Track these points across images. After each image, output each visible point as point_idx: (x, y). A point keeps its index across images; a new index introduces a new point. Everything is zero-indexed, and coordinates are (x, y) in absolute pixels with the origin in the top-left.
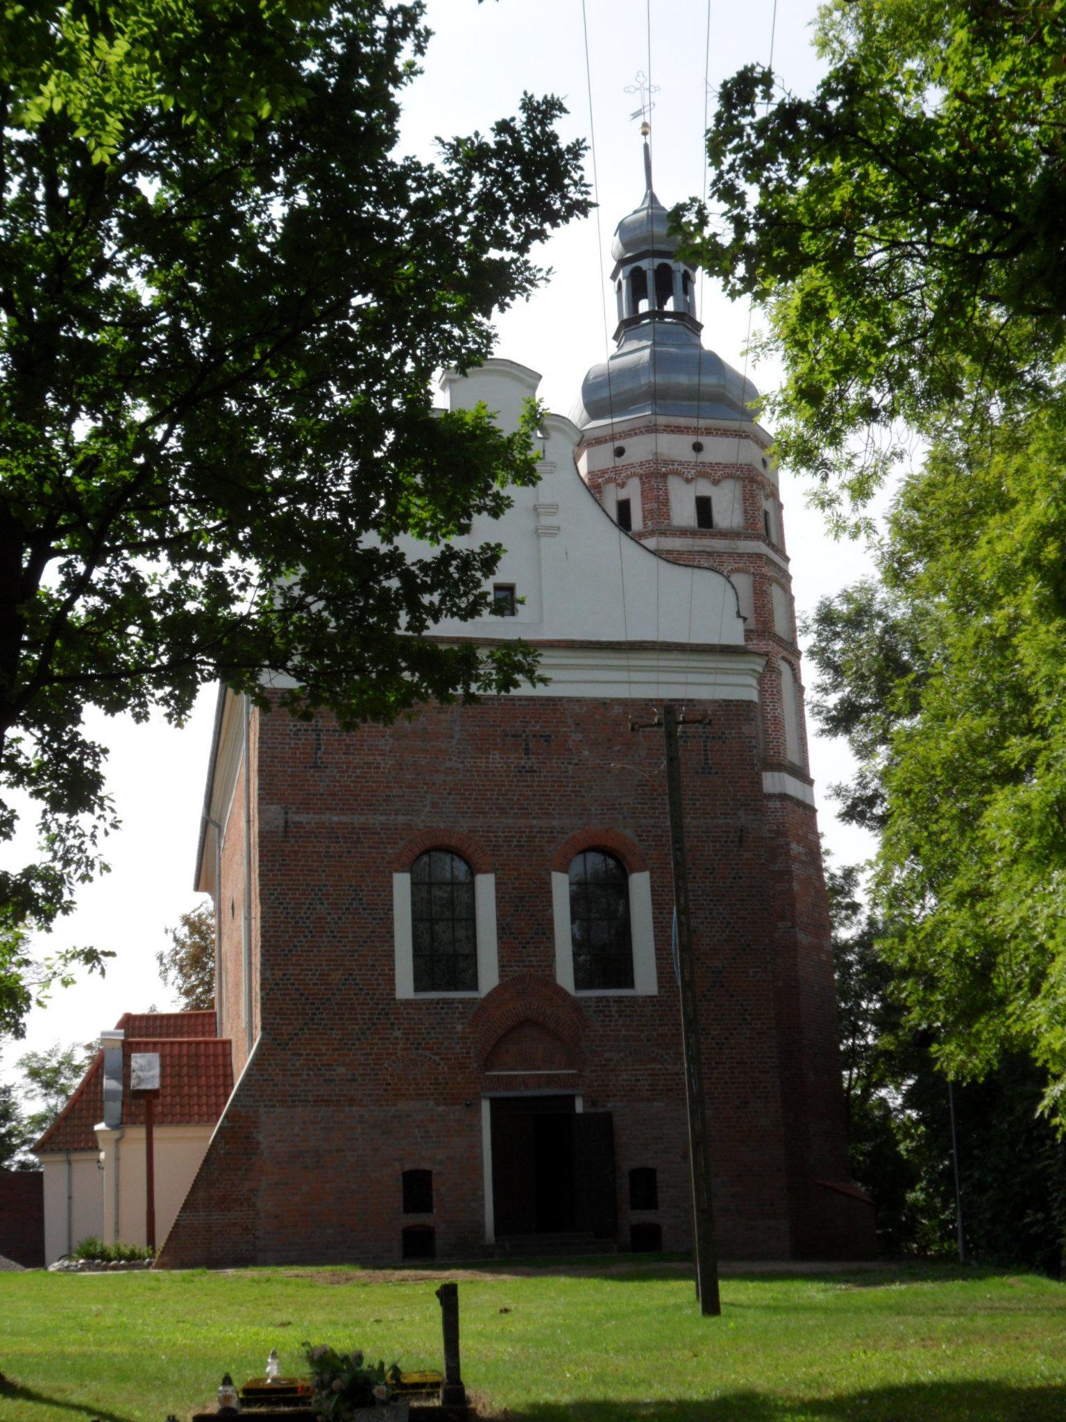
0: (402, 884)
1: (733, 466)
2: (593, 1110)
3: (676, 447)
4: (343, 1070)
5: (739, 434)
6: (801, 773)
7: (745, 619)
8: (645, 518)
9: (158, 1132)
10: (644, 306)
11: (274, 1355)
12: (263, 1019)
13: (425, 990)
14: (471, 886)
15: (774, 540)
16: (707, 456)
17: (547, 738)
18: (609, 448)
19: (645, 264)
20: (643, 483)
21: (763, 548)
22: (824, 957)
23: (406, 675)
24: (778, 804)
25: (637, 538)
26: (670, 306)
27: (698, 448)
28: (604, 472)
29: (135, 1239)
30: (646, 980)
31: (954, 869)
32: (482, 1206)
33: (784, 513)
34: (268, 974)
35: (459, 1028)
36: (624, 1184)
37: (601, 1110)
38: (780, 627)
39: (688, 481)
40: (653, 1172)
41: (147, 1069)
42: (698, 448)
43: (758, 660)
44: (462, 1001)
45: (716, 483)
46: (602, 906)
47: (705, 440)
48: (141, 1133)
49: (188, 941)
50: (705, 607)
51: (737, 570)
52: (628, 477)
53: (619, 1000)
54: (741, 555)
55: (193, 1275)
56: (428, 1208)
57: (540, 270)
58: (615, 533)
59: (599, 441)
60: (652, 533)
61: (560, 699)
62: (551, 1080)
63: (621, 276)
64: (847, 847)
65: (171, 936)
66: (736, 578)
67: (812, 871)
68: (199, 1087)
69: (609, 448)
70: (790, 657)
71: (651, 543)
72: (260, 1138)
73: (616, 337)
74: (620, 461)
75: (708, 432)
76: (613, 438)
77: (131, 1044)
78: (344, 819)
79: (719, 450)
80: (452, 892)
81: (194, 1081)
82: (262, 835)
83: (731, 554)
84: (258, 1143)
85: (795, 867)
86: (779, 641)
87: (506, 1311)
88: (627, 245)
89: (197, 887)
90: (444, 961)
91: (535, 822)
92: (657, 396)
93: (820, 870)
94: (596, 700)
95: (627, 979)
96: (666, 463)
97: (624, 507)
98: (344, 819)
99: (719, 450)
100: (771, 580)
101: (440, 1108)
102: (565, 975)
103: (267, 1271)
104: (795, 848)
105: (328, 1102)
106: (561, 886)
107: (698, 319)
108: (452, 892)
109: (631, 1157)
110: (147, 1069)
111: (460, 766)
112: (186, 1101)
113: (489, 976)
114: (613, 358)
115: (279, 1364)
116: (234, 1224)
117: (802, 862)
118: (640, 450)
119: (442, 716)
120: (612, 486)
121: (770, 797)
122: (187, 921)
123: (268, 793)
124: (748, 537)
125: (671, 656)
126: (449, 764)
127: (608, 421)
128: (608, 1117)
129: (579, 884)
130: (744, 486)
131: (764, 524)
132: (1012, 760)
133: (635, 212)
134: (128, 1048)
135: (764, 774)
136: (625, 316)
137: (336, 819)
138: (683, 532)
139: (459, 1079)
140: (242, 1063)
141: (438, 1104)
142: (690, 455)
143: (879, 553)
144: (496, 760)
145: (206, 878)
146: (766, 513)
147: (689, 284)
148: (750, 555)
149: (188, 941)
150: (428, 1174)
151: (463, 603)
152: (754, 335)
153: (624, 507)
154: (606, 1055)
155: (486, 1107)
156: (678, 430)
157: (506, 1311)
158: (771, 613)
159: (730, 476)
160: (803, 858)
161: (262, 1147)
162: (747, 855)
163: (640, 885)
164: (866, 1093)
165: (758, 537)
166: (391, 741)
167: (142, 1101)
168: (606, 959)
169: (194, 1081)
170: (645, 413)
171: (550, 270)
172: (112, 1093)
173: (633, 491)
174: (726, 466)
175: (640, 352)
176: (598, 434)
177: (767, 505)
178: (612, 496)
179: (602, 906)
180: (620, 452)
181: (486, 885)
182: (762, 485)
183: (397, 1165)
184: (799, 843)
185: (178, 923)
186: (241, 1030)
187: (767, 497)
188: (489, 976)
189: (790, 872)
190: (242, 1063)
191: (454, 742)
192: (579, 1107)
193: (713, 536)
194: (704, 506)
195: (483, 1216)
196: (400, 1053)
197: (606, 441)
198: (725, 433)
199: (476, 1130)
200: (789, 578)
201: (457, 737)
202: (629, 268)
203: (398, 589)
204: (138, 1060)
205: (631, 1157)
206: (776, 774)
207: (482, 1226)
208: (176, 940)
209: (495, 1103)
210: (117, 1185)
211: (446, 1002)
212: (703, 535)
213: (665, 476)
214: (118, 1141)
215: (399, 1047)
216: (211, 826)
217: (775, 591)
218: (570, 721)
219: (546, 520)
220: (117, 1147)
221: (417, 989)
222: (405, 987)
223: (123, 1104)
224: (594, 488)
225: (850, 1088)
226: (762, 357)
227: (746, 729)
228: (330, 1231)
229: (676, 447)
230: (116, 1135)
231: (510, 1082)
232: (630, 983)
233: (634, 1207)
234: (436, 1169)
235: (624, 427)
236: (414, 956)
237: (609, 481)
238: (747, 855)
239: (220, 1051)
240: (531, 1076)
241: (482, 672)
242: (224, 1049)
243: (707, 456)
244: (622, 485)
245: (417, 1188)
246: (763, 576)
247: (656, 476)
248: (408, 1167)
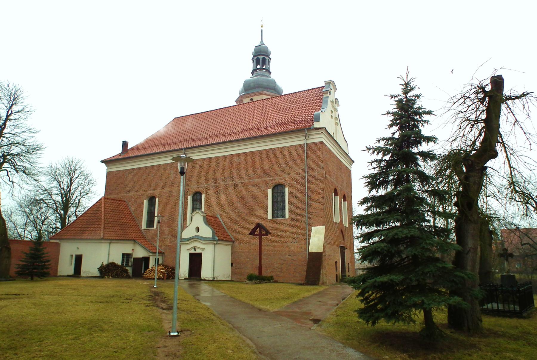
10: (258, 67)
26: (264, 67)
135: (324, 227)
202: (256, 58)
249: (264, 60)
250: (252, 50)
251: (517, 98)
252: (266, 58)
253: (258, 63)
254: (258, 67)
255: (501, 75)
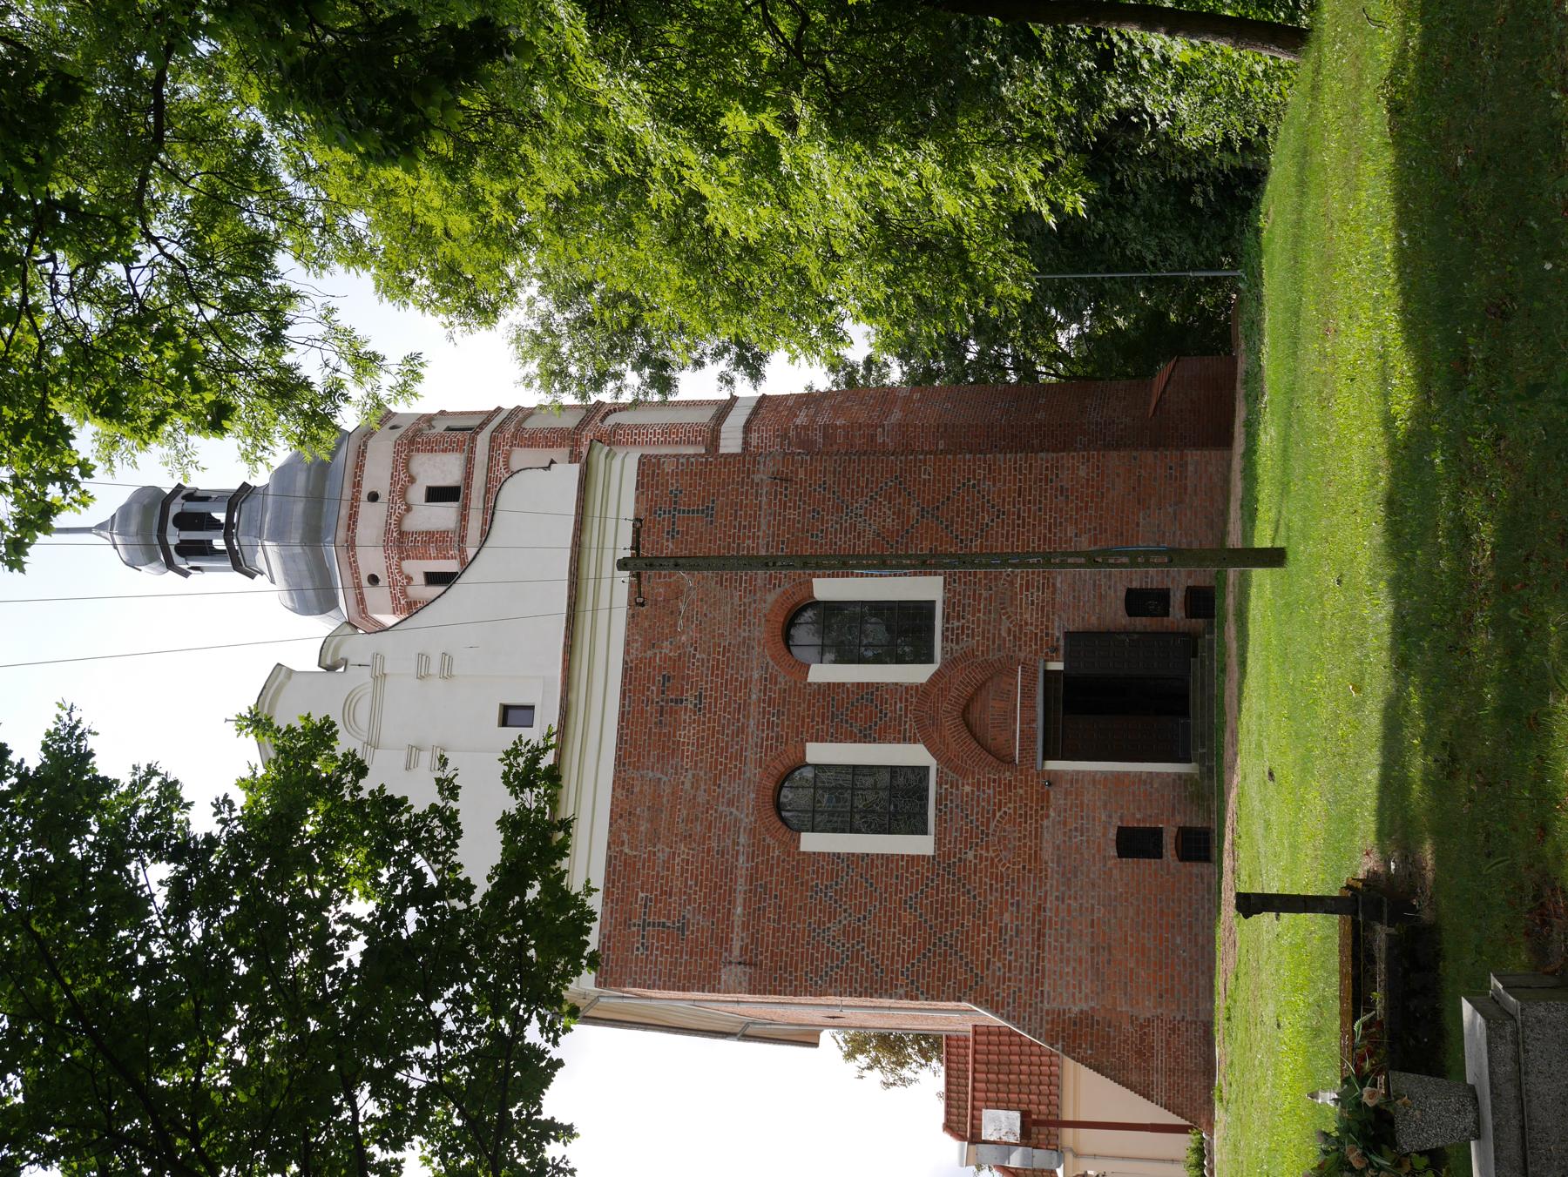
0: (812, 842)
1: (395, 461)
2: (1062, 652)
3: (372, 520)
4: (1007, 916)
5: (361, 453)
6: (724, 409)
7: (552, 462)
8: (445, 558)
9: (1068, 1116)
10: (219, 544)
11: (1313, 1096)
12: (948, 1000)
13: (925, 823)
14: (820, 768)
15: (476, 422)
16: (383, 490)
17: (666, 678)
18: (370, 592)
19: (174, 537)
20: (408, 557)
21: (483, 440)
22: (916, 396)
23: (532, 894)
24: (754, 435)
25: (466, 565)
26: (221, 516)
27: (374, 497)
28: (394, 598)
29: (1182, 1144)
30: (926, 588)
31: (801, 271)
32: (1158, 774)
33: (449, 410)
34: (901, 991)
35: (967, 789)
36: (1141, 623)
37: (1062, 643)
38: (570, 422)
39: (409, 509)
40: (1130, 591)
41: (1000, 1123)
42: (374, 497)
43: (595, 453)
44: (939, 784)
45: (412, 480)
46: (848, 631)
47: (366, 489)
48: (1068, 1135)
49: (873, 1054)
50: (540, 497)
51: (507, 464)
52: (401, 572)
53: (947, 618)
54: (490, 458)
55: (1221, 1099)
56: (1157, 833)
57: (59, 717)
58: (457, 589)
59: (361, 601)
60: (462, 551)
61: (625, 662)
62: (1028, 694)
63: (185, 567)
64: (792, 374)
65: (866, 1072)
66: (514, 466)
67: (826, 404)
68: (1021, 1063)
69: (370, 592)
70: (602, 414)
71: (471, 552)
72: (1076, 1009)
73: (252, 576)
74: (383, 581)
75: (357, 485)
76: (359, 586)
77: (972, 1135)
78: (740, 901)
79: (378, 475)
80: (824, 788)
81: (1015, 1068)
82: (753, 991)
83: (489, 470)
84: (1081, 1012)
85: (820, 421)
86: (583, 424)
87: (1271, 774)
88: (152, 559)
89: (816, 1045)
90: (897, 801)
91: (754, 697)
92: (314, 536)
93: (827, 395)
94: (628, 624)
95: (923, 610)
96: (388, 531)
97: (433, 579)
98: (740, 901)
99: (378, 475)
100: (519, 429)
101: (1052, 814)
102: (917, 674)
103: (1220, 1002)
104: (801, 419)
105: (1041, 935)
106: (824, 673)
107: (236, 487)
108: (824, 788)
109: (1114, 614)
110: (1000, 1123)
111: (690, 773)
112: (1035, 1079)
113: (914, 754)
114: (273, 581)
115: (1324, 1091)
116: (1168, 1042)
117: (816, 413)
118: (372, 559)
119: (637, 790)
120: (411, 591)
121: (746, 443)
122: (850, 1056)
123: (708, 981)
124: (472, 450)
125: (587, 544)
126: (688, 785)
127: (340, 592)
128: (1068, 635)
129: (823, 649)
130: (418, 450)
131: (459, 432)
132: (673, 201)
133: (115, 546)
134: (975, 1139)
135: (722, 451)
136: (229, 564)
137: (739, 910)
138: (463, 517)
139: (1021, 791)
140: (996, 1021)
141: (1048, 816)
142: (380, 508)
143: (458, 329)
144: (687, 734)
145: (807, 1038)
146: (449, 429)
147: (198, 494)
148: (491, 449)
149: (873, 1054)
150: (1121, 831)
151: (440, 833)
152: (166, 464)
153: (433, 579)
154: (1004, 634)
155: (1052, 765)
156: (353, 517)
157: (1271, 774)
158: (553, 430)
159: (407, 465)
160: (812, 412)
161: (1085, 1008)
162: (801, 475)
163: (827, 589)
164: (1063, 356)
165: (473, 440)
166: (659, 846)
167: (1034, 1129)
168: (904, 630)
169: (1015, 1068)
170: (332, 553)
171: (60, 706)
172: (1024, 1157)
173: (417, 568)
174: (395, 468)
175: (268, 554)
176: (352, 602)
177: (440, 427)
178: (420, 590)
179: (848, 631)
180: (374, 580)
181: (820, 753)
182: (418, 432)
183: (1110, 863)
184: (796, 416)
185: (852, 1067)
186: (960, 1018)
187: (431, 427)
188: (914, 754)
189: (826, 427)
190: (996, 1021)
191: (665, 778)
192: (1058, 666)
193: (468, 486)
194: (437, 494)
195: (1168, 774)
196: (991, 854)
197: (361, 594)
198: (359, 467)
199: (1076, 777)
200: (519, 409)
201: (659, 775)
202: (177, 559)
203: (418, 911)
204: (988, 1133)
205: (1114, 614)
206: (723, 435)
207: (1179, 776)
208: (870, 1068)
209: (1048, 756)
210: (1123, 1158)
211: (938, 802)
212: (467, 496)
213: (401, 533)
214: (1077, 1155)
215: (984, 853)
216: (749, 1031)
217: (530, 424)
218: (649, 653)
219: (435, 668)
220: (1083, 1156)
221: (924, 831)
222: (921, 845)
223: (1036, 1147)
224: (412, 608)
225: (1057, 375)
226: (194, 458)
227: (668, 468)
228: (1178, 940)
229: (372, 520)
230: (1069, 1157)
231: (1027, 737)
232: (930, 605)
233: (1167, 614)
234: (1117, 822)
235: (347, 573)
236: (890, 833)
237: (404, 593)
238: (801, 475)
239: (984, 1038)
240: (1022, 714)
241: (534, 805)
242: (982, 1034)
243: (383, 490)
244: (409, 579)
245: (1136, 843)
246: (514, 436)
247: (401, 542)
248: (1113, 852)
249: (184, 521)
250: (156, 579)
251: (971, 732)
252: (175, 509)
253: (202, 550)
254: (219, 544)
255: (1246, 917)
